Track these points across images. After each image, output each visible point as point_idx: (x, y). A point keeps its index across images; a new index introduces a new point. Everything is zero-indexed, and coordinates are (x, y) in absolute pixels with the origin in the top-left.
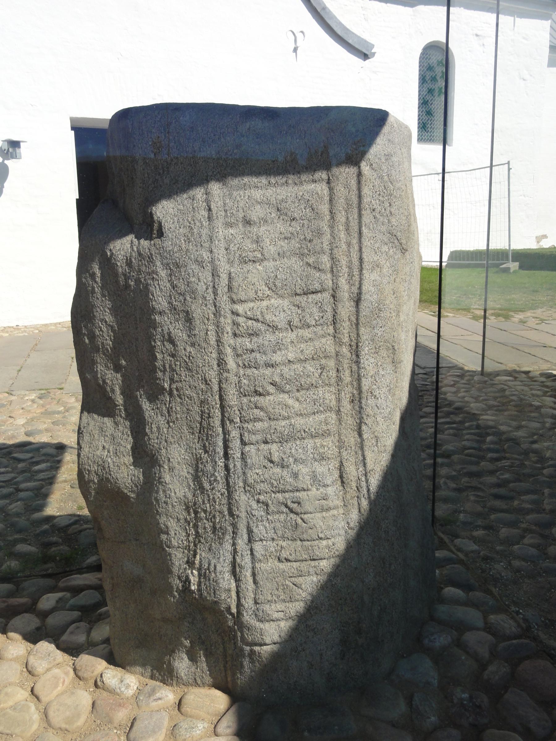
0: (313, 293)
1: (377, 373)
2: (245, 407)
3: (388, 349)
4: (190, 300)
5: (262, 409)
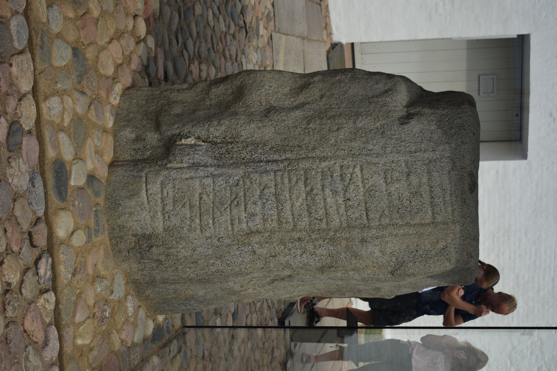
0: (367, 214)
1: (316, 255)
2: (298, 172)
3: (331, 263)
4: (363, 140)
5: (297, 182)
